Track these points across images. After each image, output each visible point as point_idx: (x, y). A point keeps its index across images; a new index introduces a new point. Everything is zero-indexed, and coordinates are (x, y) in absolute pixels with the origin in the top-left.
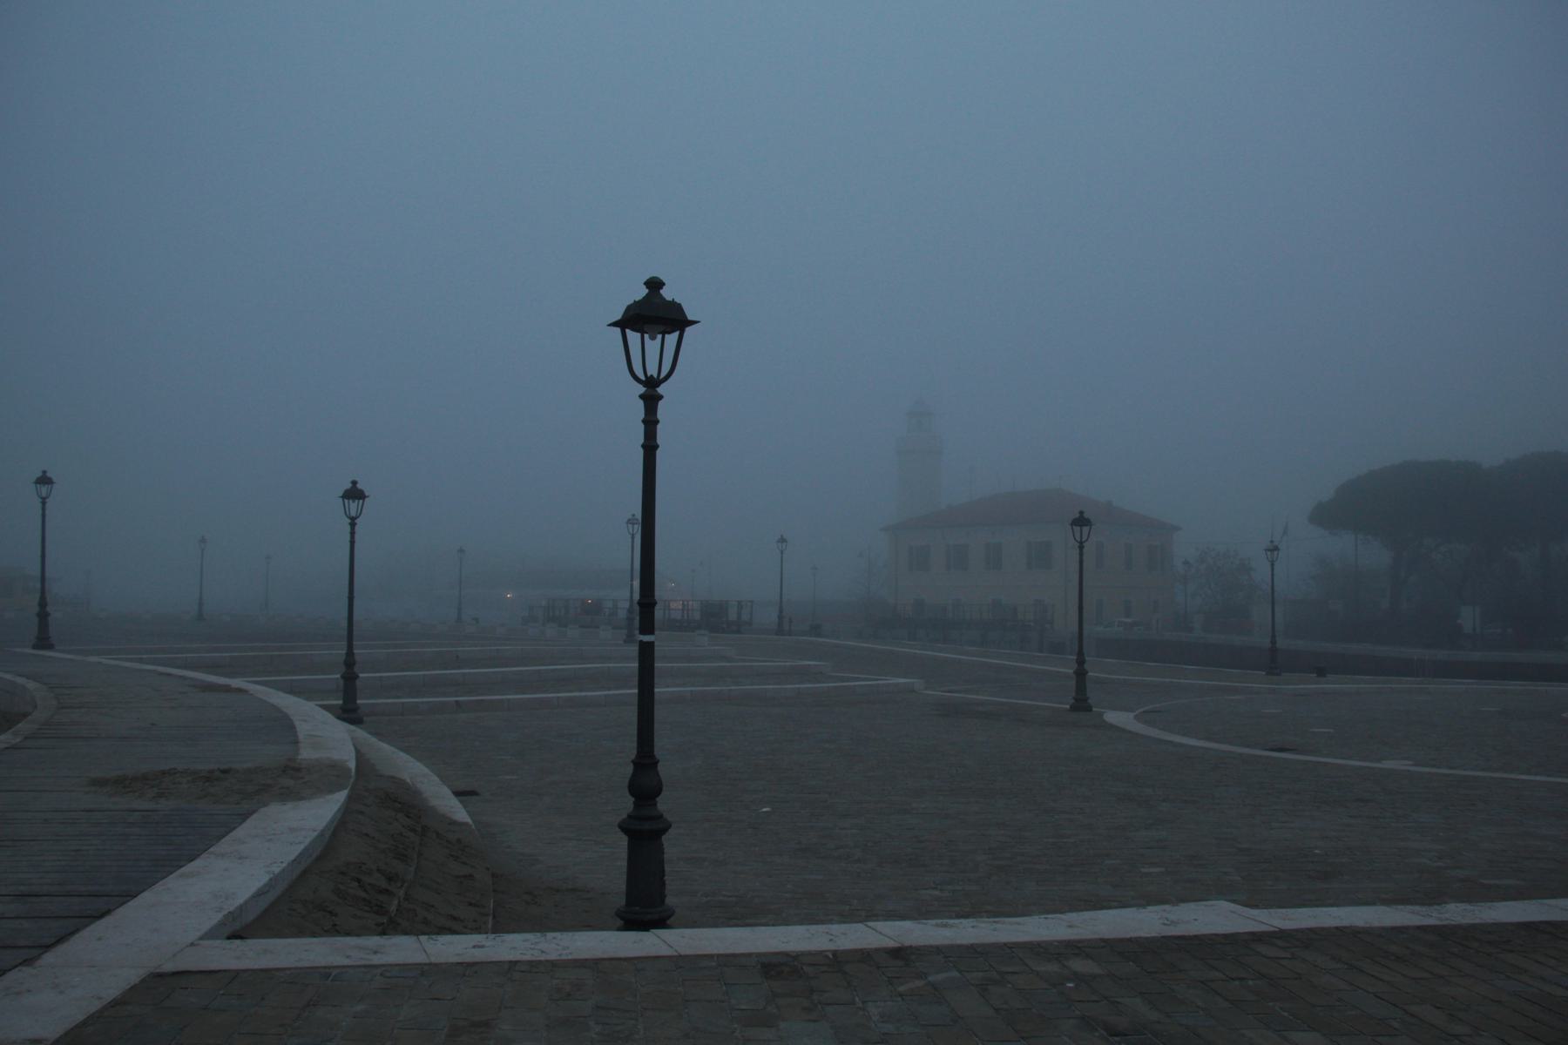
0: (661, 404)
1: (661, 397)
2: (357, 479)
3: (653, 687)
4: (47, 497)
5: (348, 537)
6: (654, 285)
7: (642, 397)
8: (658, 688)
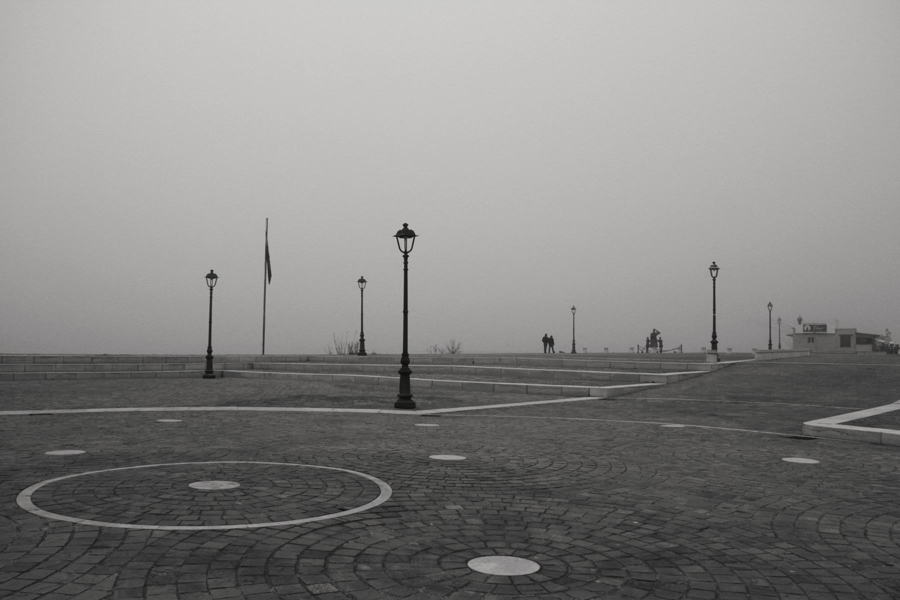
0: (408, 258)
1: (408, 256)
2: (213, 270)
3: (401, 379)
5: (209, 295)
6: (405, 225)
7: (403, 256)
8: (391, 383)
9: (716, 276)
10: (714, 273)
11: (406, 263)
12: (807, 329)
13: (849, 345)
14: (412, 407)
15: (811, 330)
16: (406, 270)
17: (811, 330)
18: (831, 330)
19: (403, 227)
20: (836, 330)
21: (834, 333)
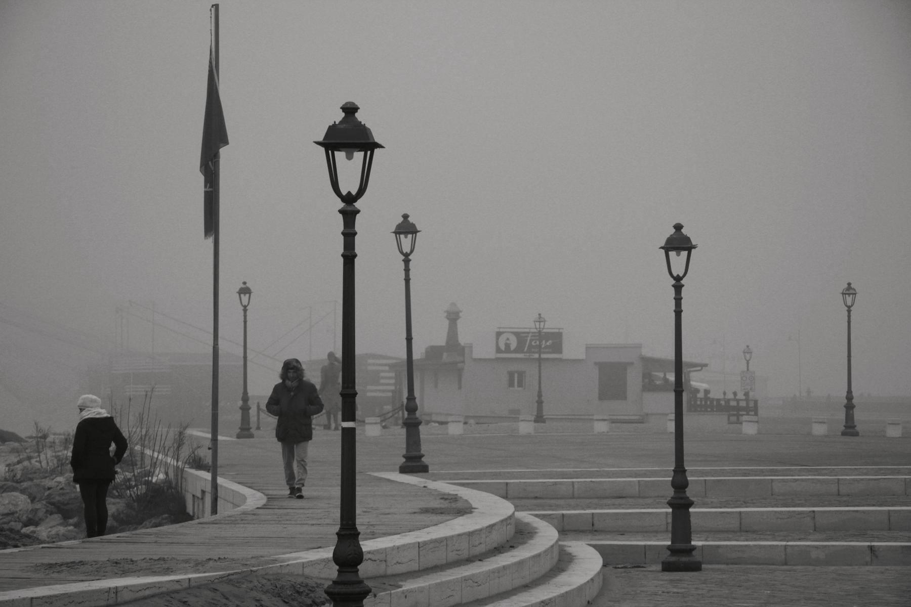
1: (410, 260)
2: (851, 282)
4: (681, 278)
9: (412, 251)
10: (406, 241)
11: (407, 270)
12: (507, 346)
13: (621, 394)
14: (423, 469)
15: (519, 350)
16: (678, 313)
17: (519, 350)
18: (572, 350)
19: (402, 219)
20: (588, 348)
21: (582, 356)
